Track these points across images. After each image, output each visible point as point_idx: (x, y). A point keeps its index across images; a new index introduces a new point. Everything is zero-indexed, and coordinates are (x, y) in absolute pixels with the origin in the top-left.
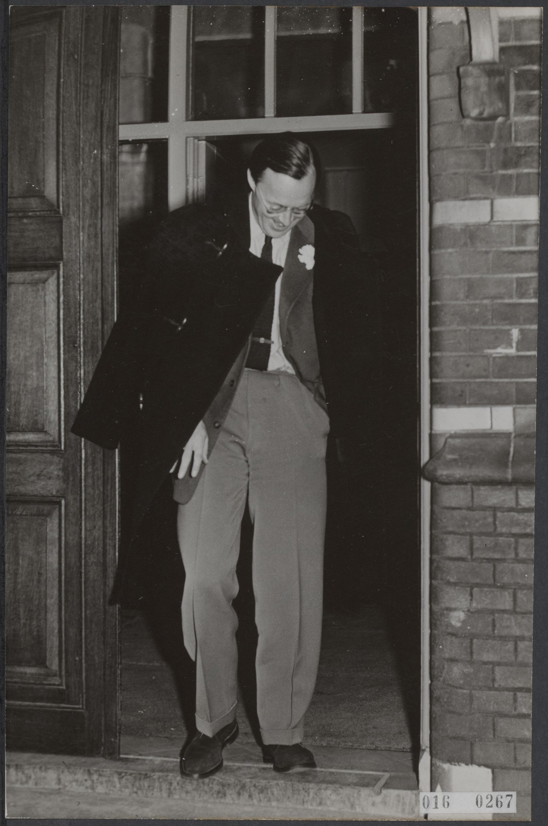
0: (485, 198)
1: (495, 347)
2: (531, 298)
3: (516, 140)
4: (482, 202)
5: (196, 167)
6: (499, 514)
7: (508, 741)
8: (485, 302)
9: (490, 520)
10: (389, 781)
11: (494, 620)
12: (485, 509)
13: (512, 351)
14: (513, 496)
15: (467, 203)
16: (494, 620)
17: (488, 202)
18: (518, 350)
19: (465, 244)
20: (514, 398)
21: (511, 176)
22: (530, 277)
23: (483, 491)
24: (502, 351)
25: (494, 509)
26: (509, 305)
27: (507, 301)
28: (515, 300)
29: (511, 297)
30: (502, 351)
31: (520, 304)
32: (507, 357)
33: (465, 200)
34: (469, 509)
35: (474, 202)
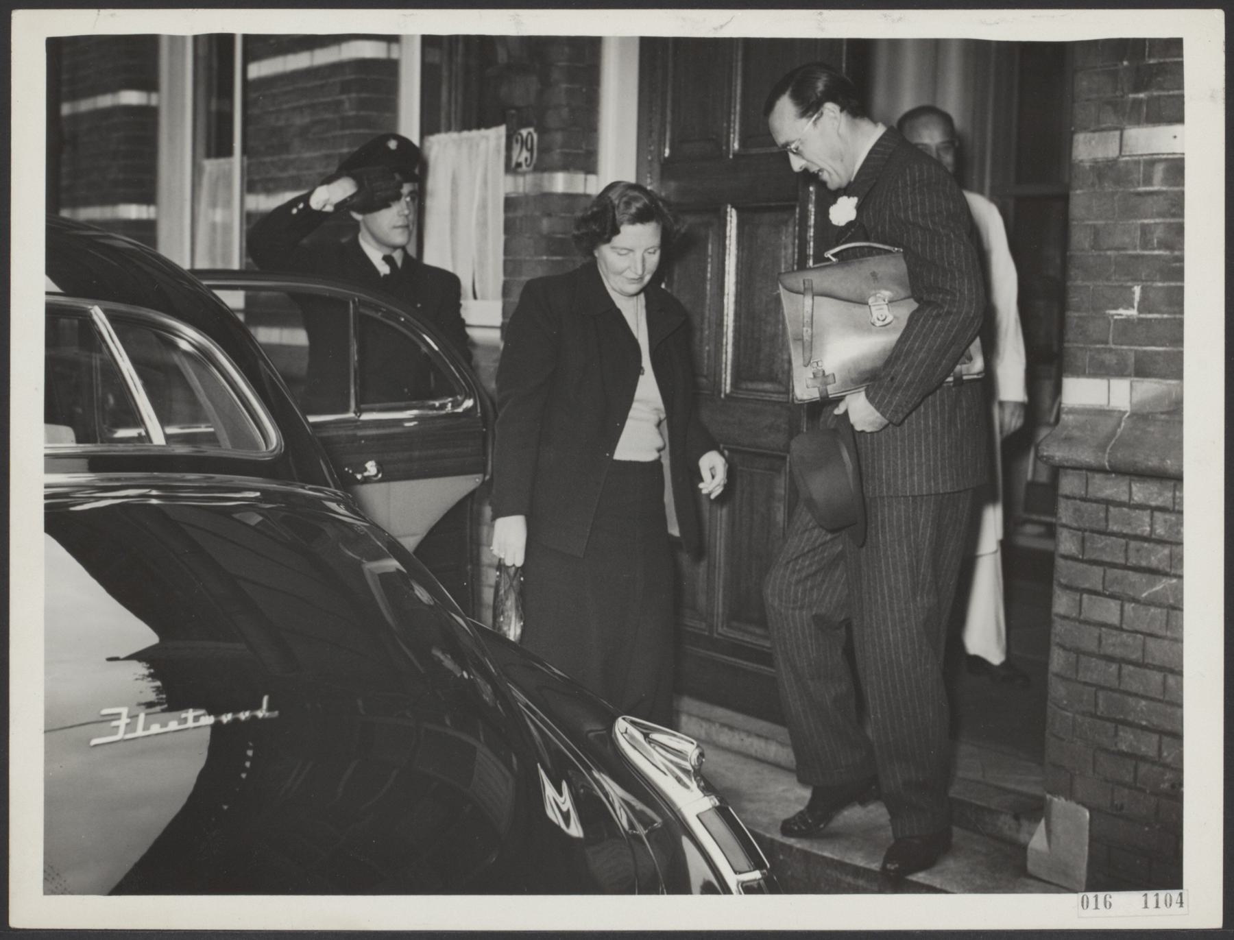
0: (1116, 129)
1: (1116, 308)
2: (231, 164)
3: (1149, 57)
4: (1112, 133)
5: (219, 239)
6: (1111, 509)
7: (1106, 781)
8: (1109, 253)
9: (1102, 515)
10: (510, 215)
11: (1100, 637)
12: (1097, 501)
13: (1133, 312)
14: (1125, 488)
15: (1097, 135)
16: (1100, 637)
17: (1117, 133)
18: (1140, 311)
19: (1093, 185)
20: (1173, 382)
21: (1140, 101)
22: (1156, 224)
23: (1098, 479)
24: (1124, 313)
25: (1108, 502)
26: (1132, 257)
27: (1131, 252)
28: (1139, 252)
29: (1135, 248)
30: (1124, 313)
31: (1143, 256)
32: (1128, 321)
33: (1094, 131)
34: (1084, 500)
35: (1105, 134)
